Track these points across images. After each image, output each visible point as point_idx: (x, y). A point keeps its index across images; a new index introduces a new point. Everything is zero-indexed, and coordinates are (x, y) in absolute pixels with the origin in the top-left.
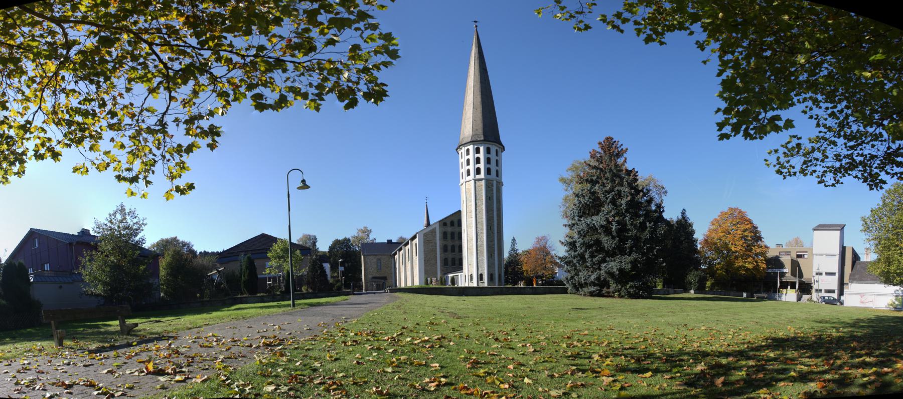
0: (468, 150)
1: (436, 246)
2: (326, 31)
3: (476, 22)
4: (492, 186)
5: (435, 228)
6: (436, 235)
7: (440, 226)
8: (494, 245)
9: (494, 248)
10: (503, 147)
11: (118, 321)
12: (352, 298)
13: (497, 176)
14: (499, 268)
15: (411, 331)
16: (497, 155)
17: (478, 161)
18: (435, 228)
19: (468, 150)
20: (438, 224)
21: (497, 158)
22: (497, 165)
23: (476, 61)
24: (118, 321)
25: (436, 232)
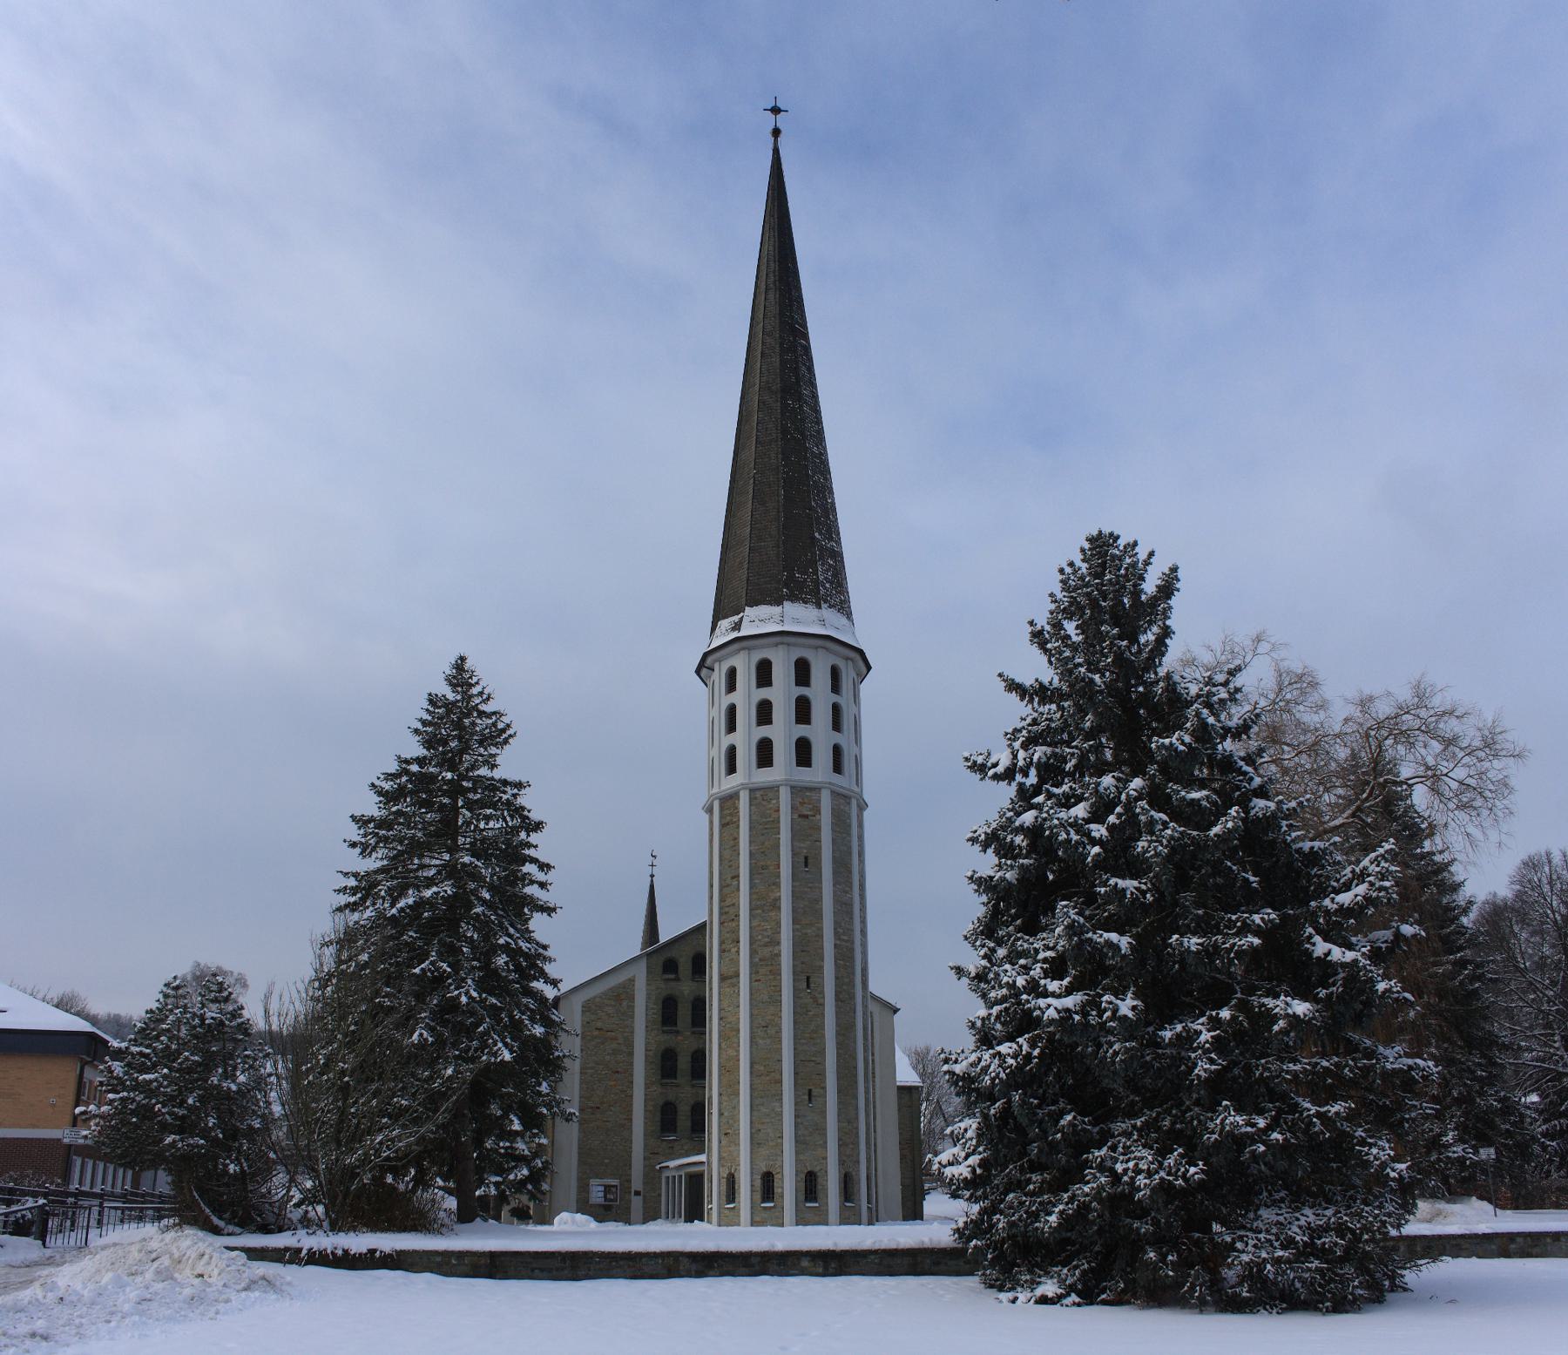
0: (732, 674)
1: (631, 1054)
2: (214, 988)
3: (776, 110)
4: (817, 811)
5: (632, 981)
6: (631, 1008)
7: (649, 971)
8: (822, 1052)
9: (822, 1063)
10: (861, 653)
11: (1492, 1150)
12: (540, 1228)
13: (838, 767)
14: (842, 1144)
15: (99, 1271)
16: (836, 688)
17: (764, 713)
18: (632, 981)
19: (732, 674)
20: (643, 965)
21: (835, 698)
22: (837, 725)
23: (771, 296)
24: (1492, 1150)
25: (632, 998)
